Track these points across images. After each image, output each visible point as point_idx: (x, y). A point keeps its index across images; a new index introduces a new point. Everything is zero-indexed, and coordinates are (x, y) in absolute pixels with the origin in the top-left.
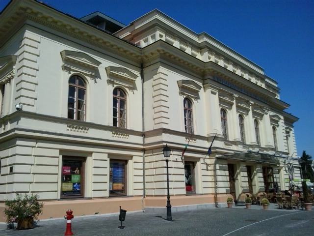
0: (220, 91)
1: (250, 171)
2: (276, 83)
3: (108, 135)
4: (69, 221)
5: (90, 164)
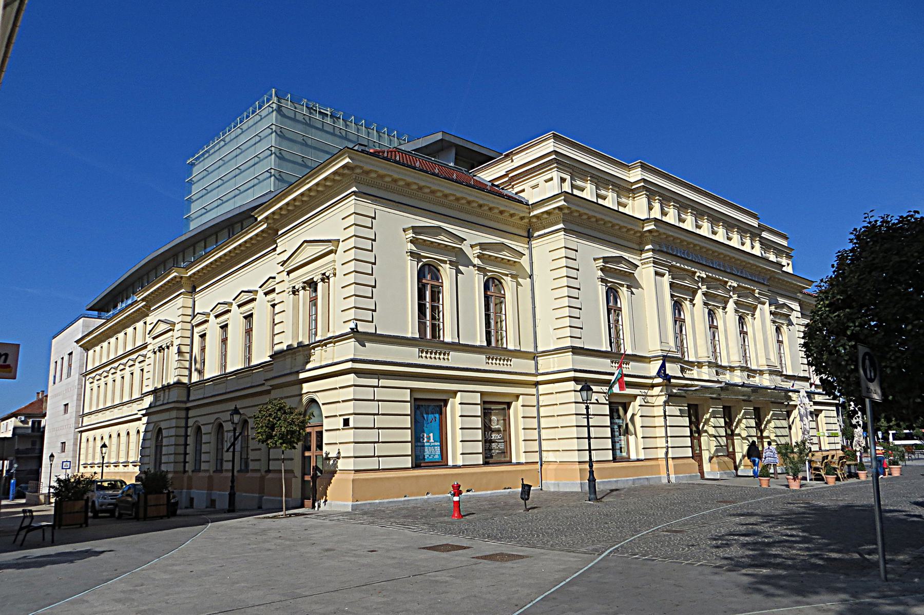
0: (671, 269)
1: (729, 414)
2: (785, 237)
3: (478, 361)
4: (456, 499)
5: (454, 410)
